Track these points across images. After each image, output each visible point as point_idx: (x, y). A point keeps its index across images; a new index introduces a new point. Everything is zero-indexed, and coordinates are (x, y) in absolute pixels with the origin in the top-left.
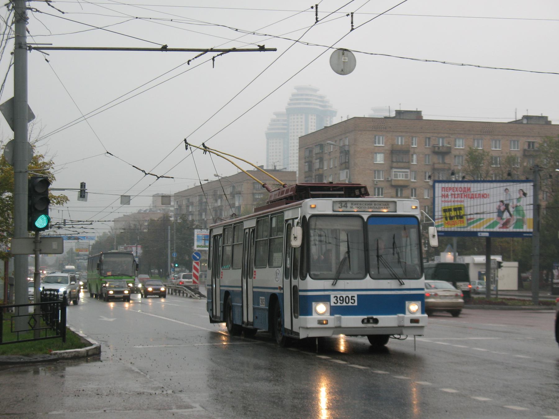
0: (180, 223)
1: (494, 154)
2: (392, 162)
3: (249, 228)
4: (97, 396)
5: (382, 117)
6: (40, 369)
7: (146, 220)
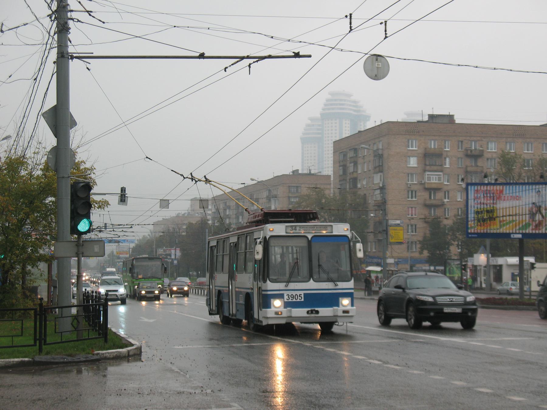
0: (217, 227)
1: (526, 157)
2: (425, 165)
3: (233, 243)
4: (138, 396)
5: (415, 121)
6: (83, 368)
7: (184, 224)
